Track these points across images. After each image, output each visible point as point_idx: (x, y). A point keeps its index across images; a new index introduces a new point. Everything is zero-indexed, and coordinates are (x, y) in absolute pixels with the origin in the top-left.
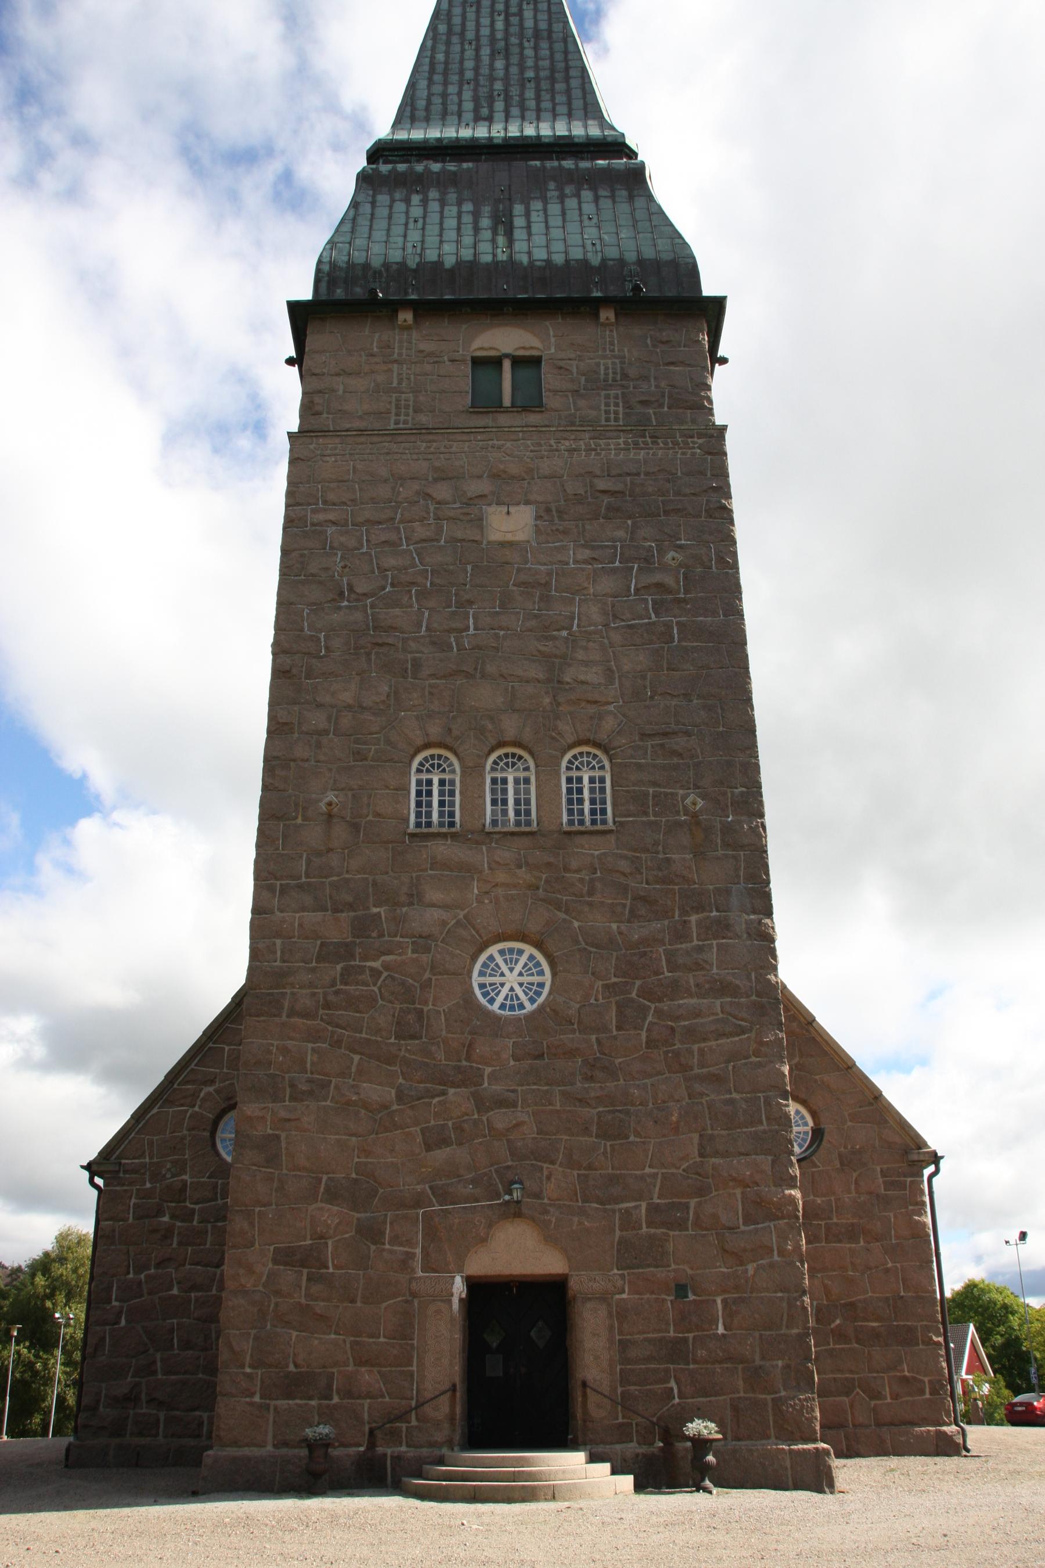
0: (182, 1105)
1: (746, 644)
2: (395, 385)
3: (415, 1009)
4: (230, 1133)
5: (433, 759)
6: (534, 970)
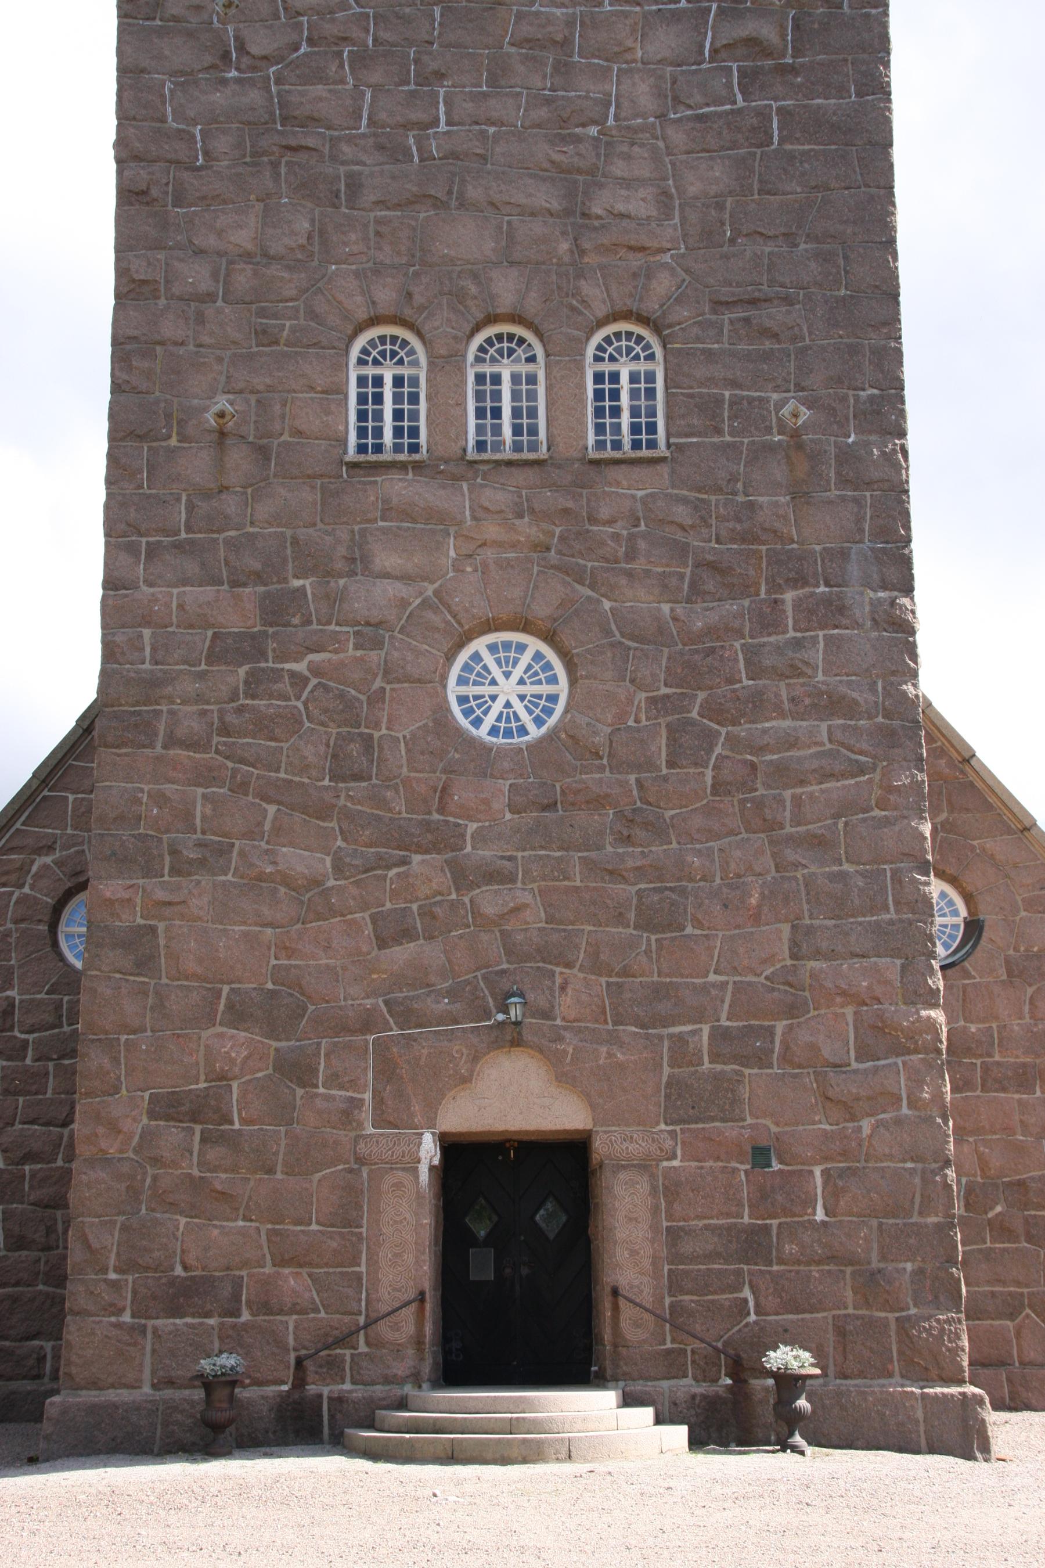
1: (891, 145)
3: (360, 734)
4: (80, 925)
5: (383, 343)
6: (542, 676)
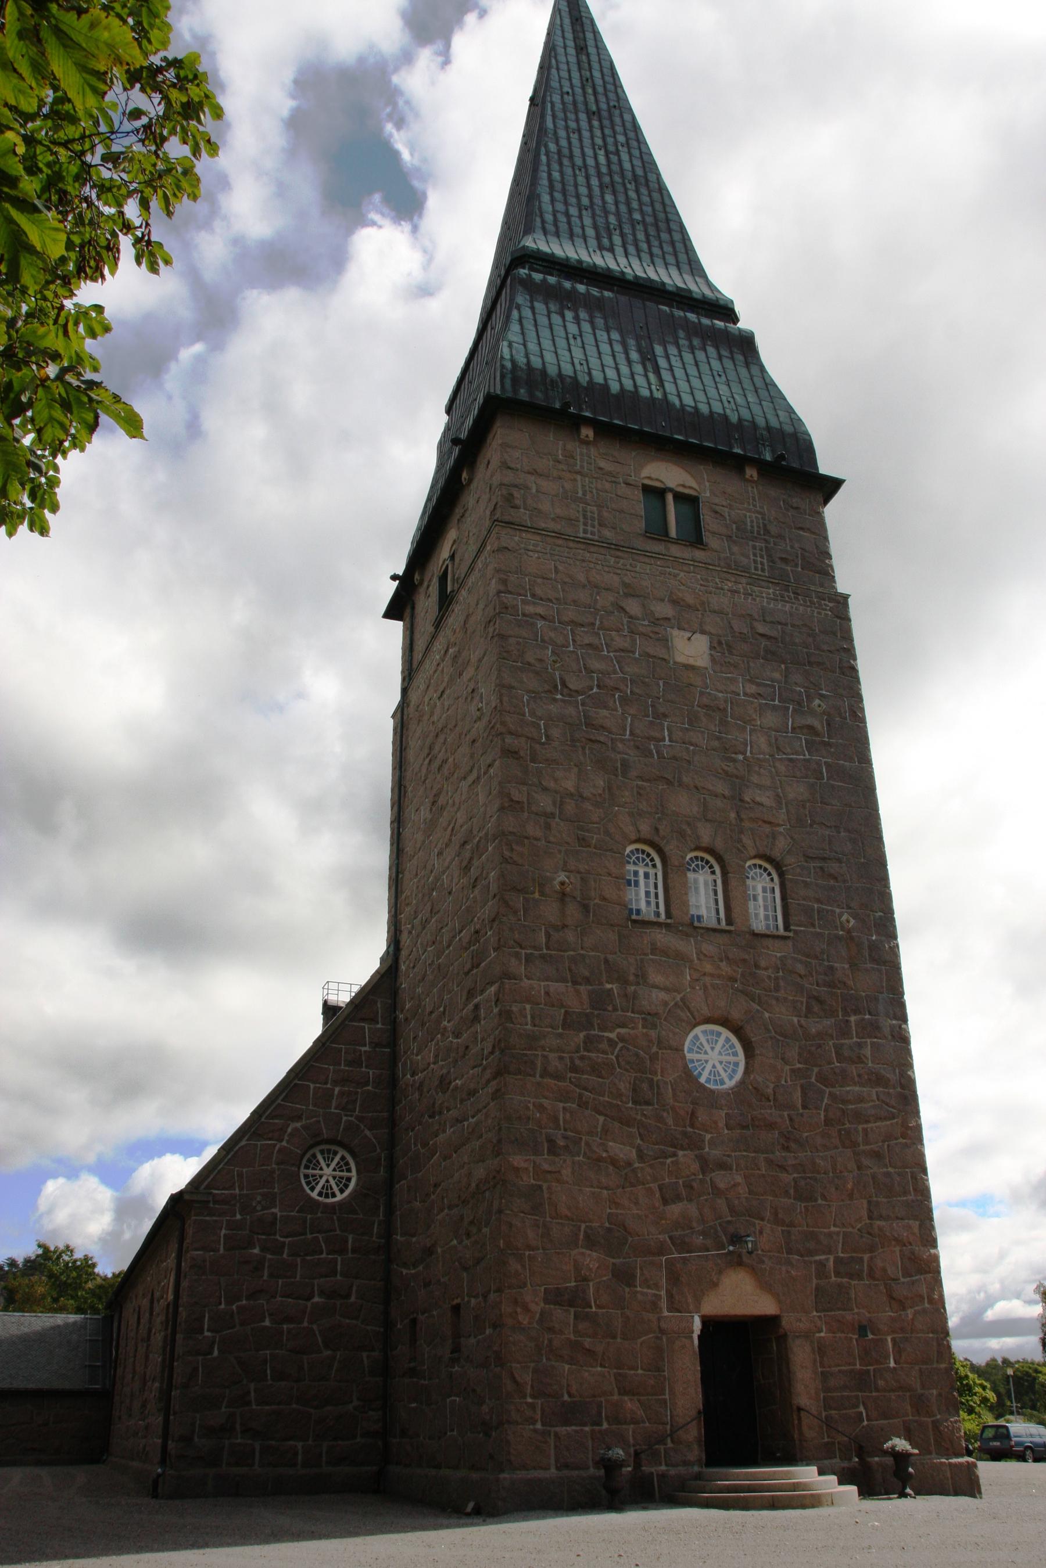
0: (270, 1139)
2: (580, 494)
